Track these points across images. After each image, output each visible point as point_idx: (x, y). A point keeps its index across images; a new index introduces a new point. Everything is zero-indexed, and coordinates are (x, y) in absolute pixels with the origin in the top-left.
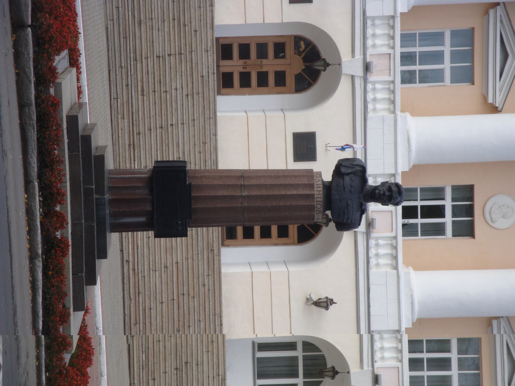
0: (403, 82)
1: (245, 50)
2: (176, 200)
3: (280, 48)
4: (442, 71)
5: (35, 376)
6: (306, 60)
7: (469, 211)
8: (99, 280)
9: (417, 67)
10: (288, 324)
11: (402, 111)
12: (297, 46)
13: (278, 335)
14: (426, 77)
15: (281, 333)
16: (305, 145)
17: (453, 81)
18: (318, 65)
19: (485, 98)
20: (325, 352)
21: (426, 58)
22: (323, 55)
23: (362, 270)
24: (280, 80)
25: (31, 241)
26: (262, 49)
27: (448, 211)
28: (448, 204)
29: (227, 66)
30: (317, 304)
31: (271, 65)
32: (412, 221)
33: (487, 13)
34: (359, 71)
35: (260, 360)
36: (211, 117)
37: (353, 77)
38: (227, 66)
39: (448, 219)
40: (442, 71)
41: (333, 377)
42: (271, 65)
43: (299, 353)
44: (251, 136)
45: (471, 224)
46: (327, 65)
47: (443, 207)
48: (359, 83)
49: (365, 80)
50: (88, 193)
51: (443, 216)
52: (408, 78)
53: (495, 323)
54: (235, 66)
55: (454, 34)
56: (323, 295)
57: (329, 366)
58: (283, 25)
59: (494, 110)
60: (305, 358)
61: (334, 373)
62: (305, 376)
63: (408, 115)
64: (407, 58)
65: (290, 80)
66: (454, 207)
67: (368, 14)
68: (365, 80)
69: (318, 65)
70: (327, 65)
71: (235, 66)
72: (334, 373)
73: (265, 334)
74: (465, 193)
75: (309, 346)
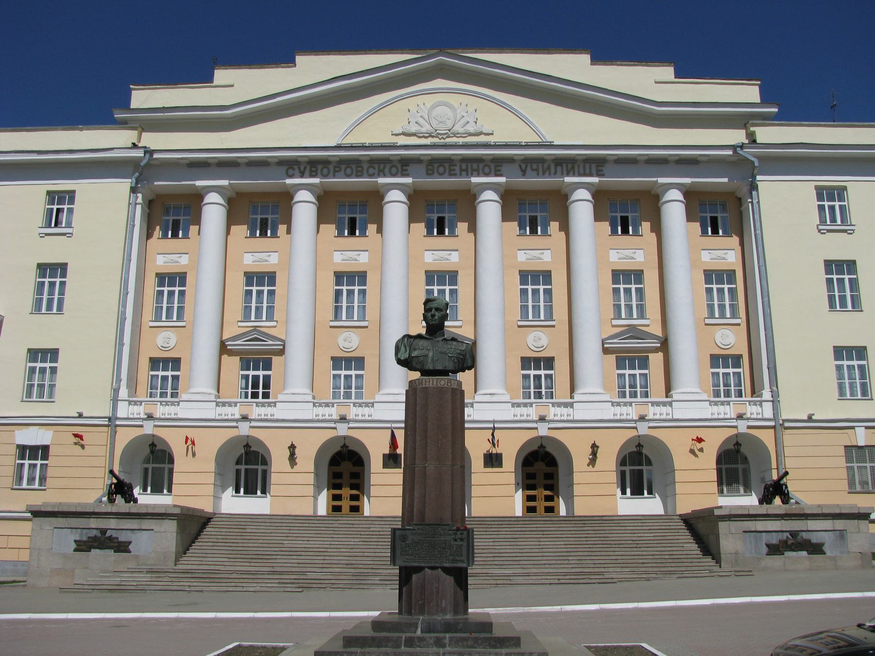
0: (268, 398)
4: (264, 376)
6: (537, 460)
7: (725, 358)
8: (491, 611)
9: (543, 390)
14: (267, 386)
15: (714, 476)
16: (391, 460)
17: (179, 370)
20: (627, 452)
21: (538, 386)
22: (339, 449)
27: (256, 373)
28: (532, 373)
29: (346, 508)
32: (543, 393)
34: (345, 426)
37: (155, 426)
38: (346, 508)
40: (264, 376)
41: (598, 447)
43: (627, 469)
46: (542, 446)
48: (254, 424)
49: (550, 421)
51: (259, 376)
52: (266, 395)
57: (732, 447)
58: (516, 472)
60: (246, 464)
64: (539, 395)
65: (356, 469)
67: (126, 416)
68: (550, 421)
70: (542, 446)
71: (346, 504)
74: (526, 363)
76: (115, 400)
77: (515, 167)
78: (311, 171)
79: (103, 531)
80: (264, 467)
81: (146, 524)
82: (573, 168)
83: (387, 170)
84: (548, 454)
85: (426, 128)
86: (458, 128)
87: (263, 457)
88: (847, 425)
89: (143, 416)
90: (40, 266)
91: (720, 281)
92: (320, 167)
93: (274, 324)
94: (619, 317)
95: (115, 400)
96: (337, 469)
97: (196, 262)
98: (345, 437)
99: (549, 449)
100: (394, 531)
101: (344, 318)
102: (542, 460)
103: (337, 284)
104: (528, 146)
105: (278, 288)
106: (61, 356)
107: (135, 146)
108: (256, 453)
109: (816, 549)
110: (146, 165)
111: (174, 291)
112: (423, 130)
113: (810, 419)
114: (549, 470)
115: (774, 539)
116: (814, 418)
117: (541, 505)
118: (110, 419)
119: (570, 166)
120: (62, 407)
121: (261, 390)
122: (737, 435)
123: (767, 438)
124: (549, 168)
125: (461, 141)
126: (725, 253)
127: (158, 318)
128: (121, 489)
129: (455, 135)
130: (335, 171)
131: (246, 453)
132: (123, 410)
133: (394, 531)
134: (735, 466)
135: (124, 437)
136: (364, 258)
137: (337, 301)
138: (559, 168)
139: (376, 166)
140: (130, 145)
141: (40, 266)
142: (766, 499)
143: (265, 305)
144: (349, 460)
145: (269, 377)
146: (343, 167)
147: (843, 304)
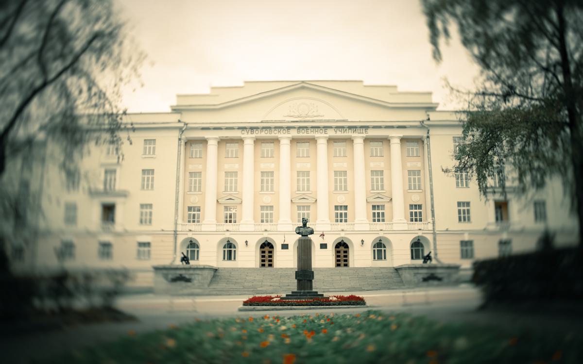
0: (384, 221)
1: (263, 261)
2: (305, 274)
3: (263, 252)
5: (280, 311)
7: (464, 203)
10: (330, 252)
11: (354, 222)
12: (337, 248)
13: (370, 254)
14: (199, 218)
15: (409, 252)
18: (342, 242)
19: (314, 203)
20: (413, 242)
22: (340, 241)
23: (355, 232)
24: (345, 252)
25: (307, 309)
26: (263, 256)
27: (304, 212)
30: (363, 244)
31: (267, 254)
33: (293, 203)
35: (227, 259)
36: (354, 269)
37: (193, 234)
39: (380, 211)
42: (342, 254)
43: (376, 249)
44: (286, 260)
45: (344, 206)
46: (342, 241)
47: (303, 213)
49: (270, 231)
50: (300, 295)
53: (368, 201)
54: (342, 263)
55: (298, 210)
56: (361, 242)
59: (316, 200)
60: (191, 248)
61: (380, 240)
62: (382, 247)
63: (393, 220)
66: (303, 210)
67: (330, 230)
68: (268, 231)
69: (267, 243)
70: (342, 241)
71: (267, 263)
72: (380, 240)
73: (409, 256)
75: (374, 247)
76: (176, 224)
77: (296, 130)
78: (251, 132)
79: (181, 275)
80: (235, 249)
81: (198, 272)
82: (356, 130)
83: (281, 132)
84: (345, 243)
85: (297, 114)
86: (310, 114)
87: (197, 245)
88: (461, 233)
89: (187, 230)
90: (143, 170)
91: (303, 176)
92: (255, 130)
93: (273, 193)
94: (373, 189)
95: (176, 224)
96: (263, 250)
97: (205, 168)
98: (266, 238)
99: (269, 241)
100: (296, 272)
101: (229, 190)
102: (343, 246)
103: (262, 176)
104: (337, 121)
105: (275, 178)
106: (154, 207)
107: (179, 121)
108: (195, 244)
109: (439, 279)
110: (185, 129)
111: (304, 179)
112: (296, 115)
113: (447, 230)
114: (346, 249)
115: (425, 276)
116: (449, 230)
117: (267, 263)
118: (174, 231)
119: (354, 129)
120: (156, 226)
121: (343, 218)
122: (419, 236)
123: (430, 237)
124: (346, 130)
125: (311, 119)
126: (415, 164)
127: (190, 191)
128: (185, 259)
129: (308, 117)
130: (261, 132)
131: (191, 244)
132: (179, 228)
133: (296, 272)
134: (381, 249)
135: (181, 238)
136: (309, 165)
137: (262, 183)
138: (350, 130)
139: (277, 130)
140: (177, 121)
141: (143, 170)
142: (425, 262)
143: (229, 185)
144: (268, 246)
145: (199, 214)
146: (264, 130)
147: (462, 185)
